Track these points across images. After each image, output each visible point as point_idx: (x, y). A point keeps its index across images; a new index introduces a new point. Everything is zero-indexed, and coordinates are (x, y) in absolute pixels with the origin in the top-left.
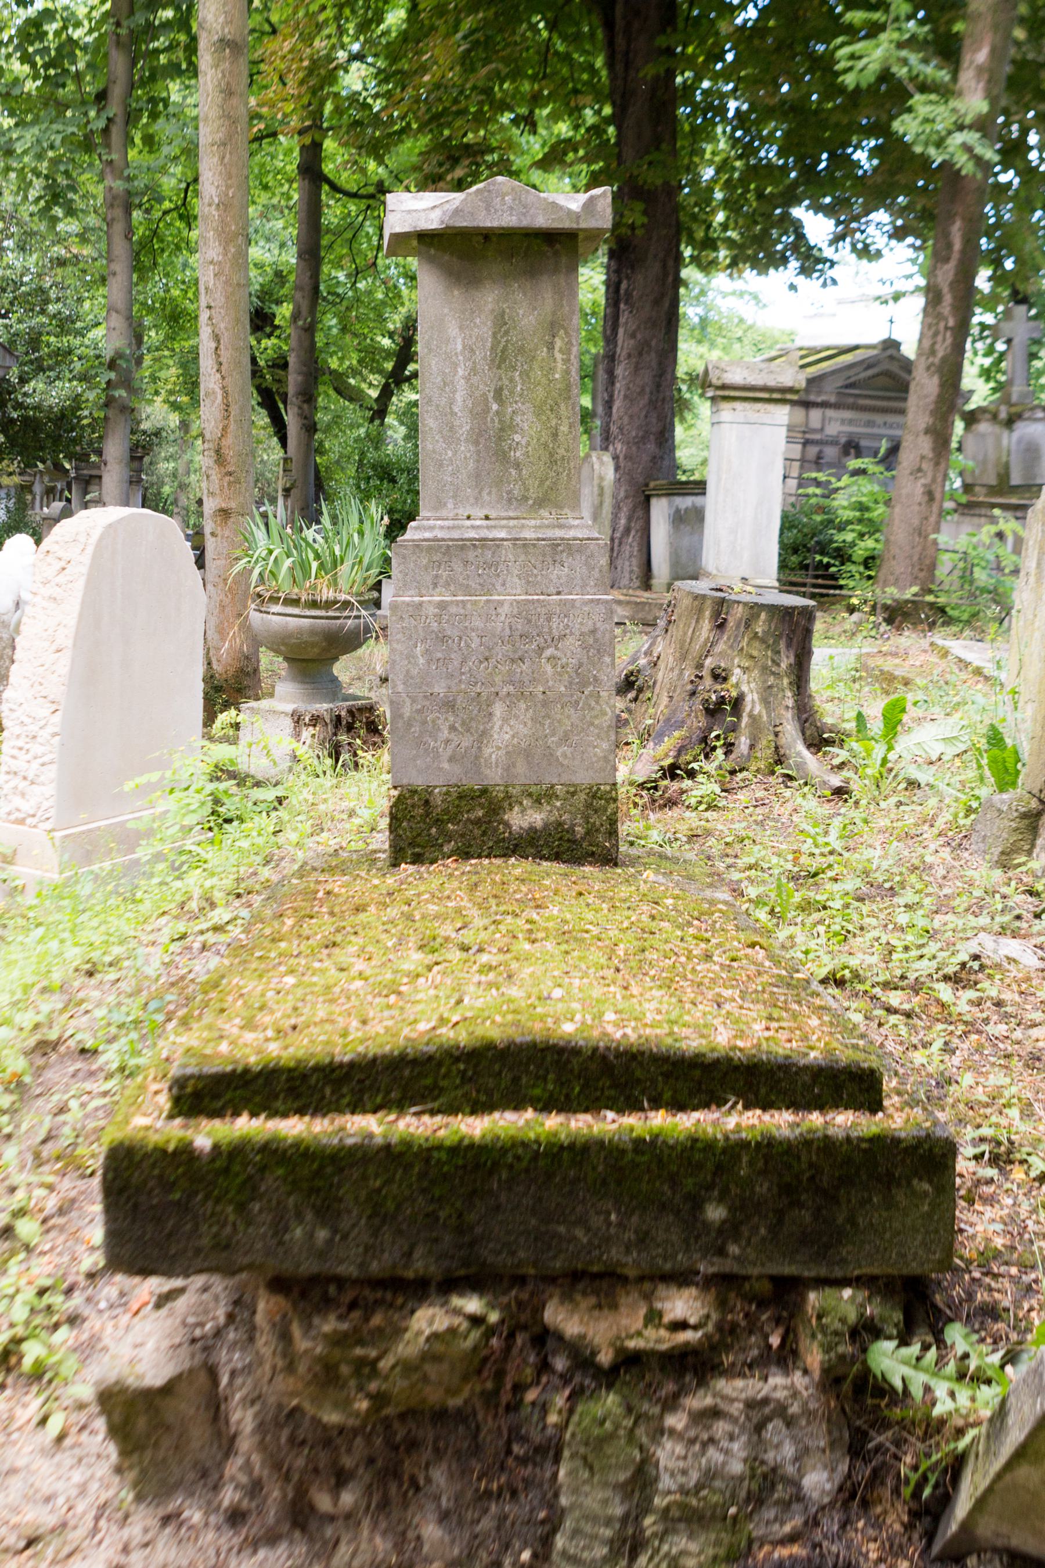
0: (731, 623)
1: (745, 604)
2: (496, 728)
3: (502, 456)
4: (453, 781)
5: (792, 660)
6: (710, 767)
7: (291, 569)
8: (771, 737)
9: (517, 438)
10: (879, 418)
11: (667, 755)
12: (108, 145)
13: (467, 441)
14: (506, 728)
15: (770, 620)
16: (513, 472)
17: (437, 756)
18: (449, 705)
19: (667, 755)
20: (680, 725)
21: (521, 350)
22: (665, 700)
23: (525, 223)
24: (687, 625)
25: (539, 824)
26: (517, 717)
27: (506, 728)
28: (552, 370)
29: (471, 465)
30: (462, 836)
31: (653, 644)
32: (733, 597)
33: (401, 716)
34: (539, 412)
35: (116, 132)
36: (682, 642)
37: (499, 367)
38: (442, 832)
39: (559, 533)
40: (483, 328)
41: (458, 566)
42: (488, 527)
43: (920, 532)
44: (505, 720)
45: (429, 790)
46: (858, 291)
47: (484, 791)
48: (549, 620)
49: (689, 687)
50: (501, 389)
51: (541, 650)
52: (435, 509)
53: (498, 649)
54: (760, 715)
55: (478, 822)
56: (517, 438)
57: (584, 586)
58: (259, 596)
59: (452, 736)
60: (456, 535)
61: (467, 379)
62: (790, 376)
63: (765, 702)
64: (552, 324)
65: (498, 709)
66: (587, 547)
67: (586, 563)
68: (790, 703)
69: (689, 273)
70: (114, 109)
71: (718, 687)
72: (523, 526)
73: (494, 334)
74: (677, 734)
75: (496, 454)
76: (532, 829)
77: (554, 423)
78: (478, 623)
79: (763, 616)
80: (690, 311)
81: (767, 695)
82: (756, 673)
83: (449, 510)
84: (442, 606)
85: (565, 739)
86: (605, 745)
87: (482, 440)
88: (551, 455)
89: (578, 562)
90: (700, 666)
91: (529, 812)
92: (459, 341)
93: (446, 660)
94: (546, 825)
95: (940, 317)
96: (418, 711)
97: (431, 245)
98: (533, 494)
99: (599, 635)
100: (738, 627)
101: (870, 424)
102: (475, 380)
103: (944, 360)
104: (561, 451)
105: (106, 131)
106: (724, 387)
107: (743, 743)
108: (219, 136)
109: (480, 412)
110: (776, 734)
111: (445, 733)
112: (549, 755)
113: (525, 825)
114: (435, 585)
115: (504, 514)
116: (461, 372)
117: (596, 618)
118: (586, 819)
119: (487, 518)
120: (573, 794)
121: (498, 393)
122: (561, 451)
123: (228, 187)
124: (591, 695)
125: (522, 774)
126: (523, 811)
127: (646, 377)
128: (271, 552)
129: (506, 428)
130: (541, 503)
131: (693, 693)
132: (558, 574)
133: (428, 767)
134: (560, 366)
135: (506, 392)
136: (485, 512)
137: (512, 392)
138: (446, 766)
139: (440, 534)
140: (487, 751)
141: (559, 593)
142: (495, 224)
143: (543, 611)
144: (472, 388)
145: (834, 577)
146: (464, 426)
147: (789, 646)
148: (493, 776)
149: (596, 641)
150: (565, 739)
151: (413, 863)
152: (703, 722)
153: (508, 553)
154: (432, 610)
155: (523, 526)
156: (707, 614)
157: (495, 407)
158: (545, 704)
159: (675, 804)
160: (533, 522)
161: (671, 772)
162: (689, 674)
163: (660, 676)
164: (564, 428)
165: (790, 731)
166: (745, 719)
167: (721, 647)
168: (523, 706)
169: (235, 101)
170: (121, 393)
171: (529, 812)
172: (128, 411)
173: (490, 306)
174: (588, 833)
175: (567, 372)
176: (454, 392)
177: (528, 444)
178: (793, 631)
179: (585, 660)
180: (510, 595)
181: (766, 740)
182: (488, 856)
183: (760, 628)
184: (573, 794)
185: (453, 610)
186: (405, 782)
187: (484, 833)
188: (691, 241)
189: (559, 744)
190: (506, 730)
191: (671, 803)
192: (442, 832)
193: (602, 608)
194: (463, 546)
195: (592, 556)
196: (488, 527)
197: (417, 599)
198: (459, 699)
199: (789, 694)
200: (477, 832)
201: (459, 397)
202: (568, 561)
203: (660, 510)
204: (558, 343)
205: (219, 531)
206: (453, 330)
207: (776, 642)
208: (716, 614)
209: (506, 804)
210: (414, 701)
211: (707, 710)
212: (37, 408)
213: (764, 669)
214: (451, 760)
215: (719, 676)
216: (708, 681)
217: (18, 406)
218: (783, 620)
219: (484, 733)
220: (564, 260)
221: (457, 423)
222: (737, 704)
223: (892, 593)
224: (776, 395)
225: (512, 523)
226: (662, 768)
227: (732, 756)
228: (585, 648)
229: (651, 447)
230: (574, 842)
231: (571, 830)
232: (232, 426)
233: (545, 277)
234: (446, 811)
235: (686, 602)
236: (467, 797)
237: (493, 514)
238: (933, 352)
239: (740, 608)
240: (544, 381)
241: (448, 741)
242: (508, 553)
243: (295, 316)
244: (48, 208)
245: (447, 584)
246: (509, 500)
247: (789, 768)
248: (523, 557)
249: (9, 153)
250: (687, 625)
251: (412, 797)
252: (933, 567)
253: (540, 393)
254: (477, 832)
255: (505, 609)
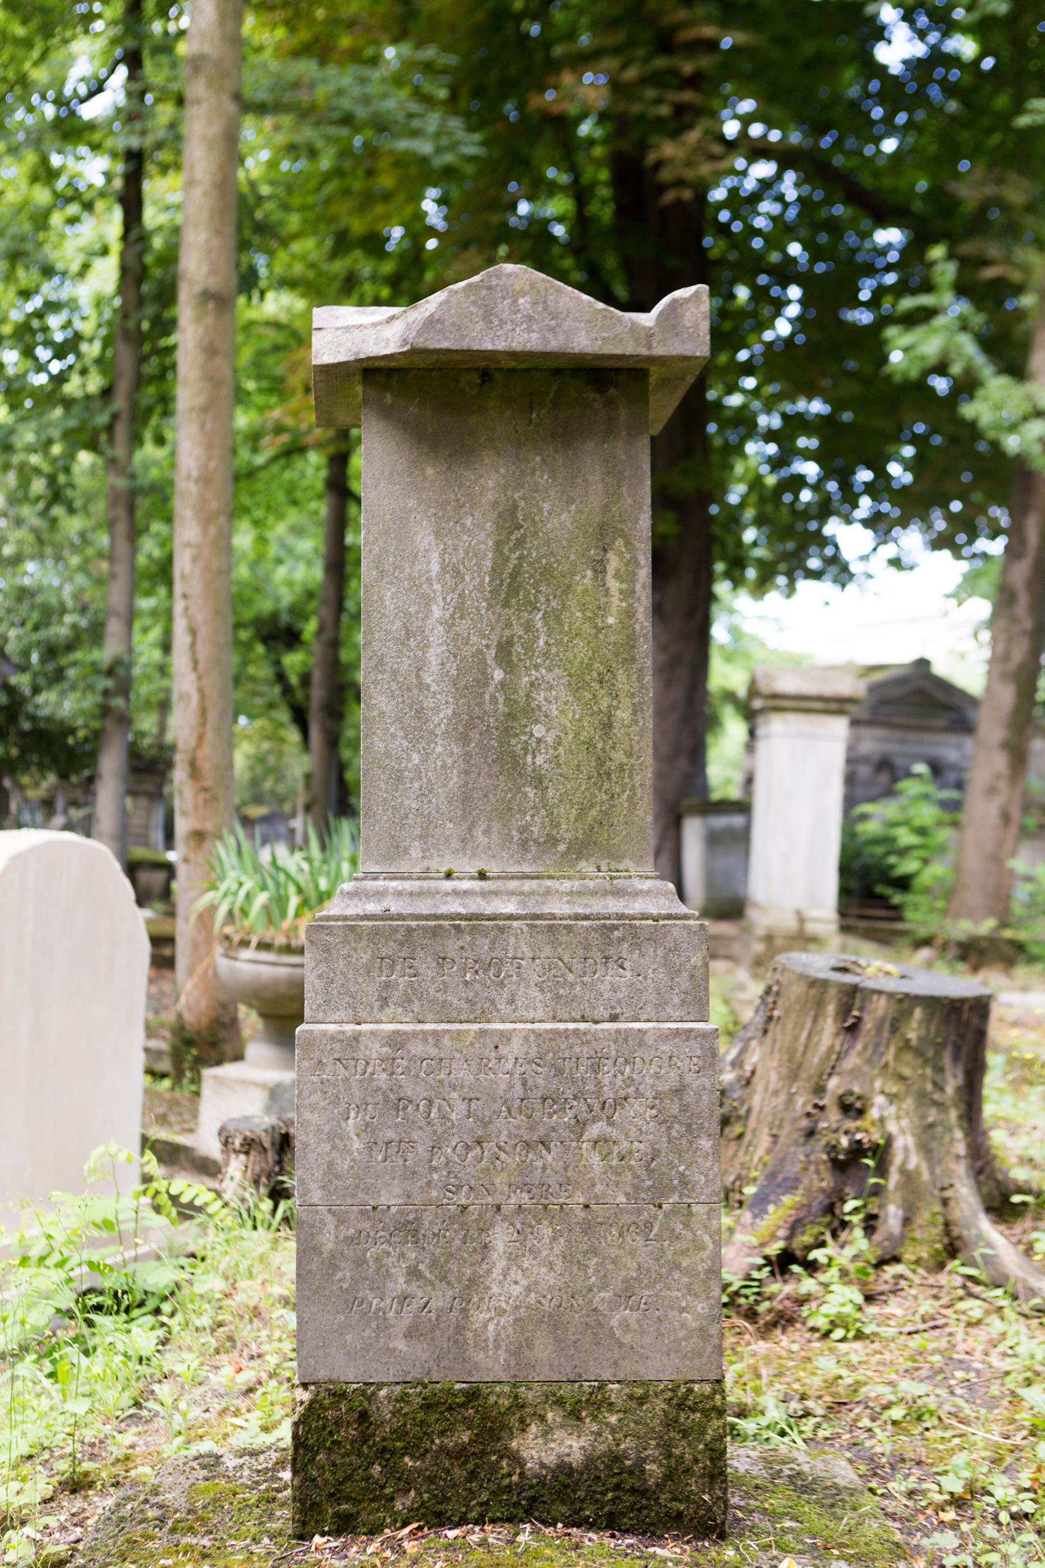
0: (868, 1025)
1: (891, 995)
2: (497, 1273)
3: (510, 764)
4: (414, 1374)
5: (960, 1080)
6: (844, 1257)
7: (266, 908)
8: (937, 1208)
9: (538, 731)
10: (913, 736)
11: (773, 1237)
12: (111, 440)
13: (447, 734)
14: (515, 1274)
15: (927, 1020)
16: (530, 792)
17: (384, 1328)
18: (408, 1229)
19: (773, 1237)
20: (791, 1185)
21: (546, 574)
22: (764, 1141)
23: (554, 344)
24: (799, 1026)
25: (576, 1458)
26: (534, 1252)
27: (515, 1274)
28: (603, 609)
29: (455, 779)
30: (431, 1480)
31: (743, 1051)
32: (870, 984)
33: (317, 1250)
34: (577, 685)
35: (121, 431)
36: (791, 1052)
37: (506, 604)
38: (392, 1471)
39: (614, 906)
40: (479, 535)
41: (427, 968)
42: (484, 894)
43: (996, 859)
44: (513, 1259)
45: (368, 1391)
46: (904, 601)
47: (473, 1395)
48: (596, 1068)
49: (804, 1123)
50: (510, 643)
51: (580, 1125)
52: (388, 858)
53: (500, 1123)
54: (917, 1172)
55: (460, 1454)
56: (538, 731)
57: (660, 1006)
58: (227, 938)
59: (413, 1288)
60: (424, 908)
61: (449, 625)
62: (848, 686)
63: (925, 1148)
64: (602, 527)
65: (500, 1237)
66: (666, 931)
67: (666, 963)
68: (961, 1148)
69: (722, 588)
70: (119, 403)
71: (851, 1124)
72: (548, 892)
73: (498, 546)
74: (787, 1200)
75: (499, 759)
76: (563, 1468)
77: (604, 704)
78: (463, 1074)
79: (918, 1013)
80: (719, 632)
81: (928, 1138)
82: (909, 1103)
83: (414, 860)
84: (397, 1041)
85: (626, 1294)
86: (701, 1307)
87: (474, 735)
88: (600, 762)
89: (650, 959)
90: (820, 1090)
91: (558, 1434)
92: (435, 557)
93: (403, 1144)
94: (590, 1461)
95: (1014, 620)
96: (350, 1240)
97: (386, 387)
98: (566, 833)
99: (689, 1097)
100: (879, 1029)
101: (903, 742)
102: (463, 626)
103: (1021, 667)
104: (619, 756)
105: (110, 428)
106: (775, 696)
107: (892, 1215)
108: (200, 400)
109: (470, 684)
110: (945, 1202)
111: (399, 1283)
112: (595, 1325)
113: (551, 1460)
114: (384, 1002)
115: (514, 869)
116: (437, 612)
117: (684, 1065)
118: (667, 1448)
119: (482, 876)
120: (642, 1400)
121: (505, 649)
122: (619, 756)
123: (209, 459)
124: (675, 1212)
125: (545, 1360)
126: (546, 1434)
127: (678, 692)
128: (241, 884)
129: (519, 713)
130: (580, 850)
131: (811, 1133)
132: (612, 981)
133: (367, 1348)
134: (616, 602)
135: (518, 648)
136: (479, 865)
137: (529, 649)
138: (400, 1344)
139: (395, 906)
140: (479, 1317)
141: (614, 1018)
142: (501, 346)
143: (586, 1051)
144: (456, 642)
145: (896, 908)
146: (442, 709)
147: (956, 1058)
148: (490, 1365)
149: (684, 1108)
150: (626, 1294)
151: (337, 1533)
152: (827, 1182)
153: (520, 943)
154: (376, 1050)
155: (548, 892)
156: (831, 1008)
157: (498, 675)
158: (587, 1228)
159: (791, 1321)
160: (566, 885)
161: (783, 1264)
162: (802, 1102)
163: (756, 1101)
164: (623, 715)
165: (966, 1198)
166: (894, 1178)
167: (852, 1061)
168: (546, 1231)
169: (219, 361)
170: (118, 702)
171: (558, 1434)
172: (125, 721)
173: (491, 496)
174: (669, 1476)
175: (629, 613)
176: (425, 647)
177: (558, 741)
178: (961, 1036)
179: (664, 1145)
180: (523, 1022)
181: (928, 1212)
182: (479, 1521)
183: (913, 1032)
184: (642, 1400)
185: (417, 1048)
186: (322, 1375)
187: (473, 1475)
188: (724, 558)
189: (614, 1306)
190: (515, 1279)
191: (784, 1320)
192: (392, 1471)
193: (694, 1047)
194: (438, 929)
195: (676, 948)
196: (484, 894)
197: (349, 1027)
198: (427, 1218)
199: (959, 1134)
200: (459, 1473)
201: (434, 656)
202: (632, 958)
203: (693, 831)
204: (613, 563)
205: (192, 856)
206: (424, 538)
207: (938, 1054)
208: (845, 1010)
209: (513, 1421)
210: (341, 1220)
211: (834, 1161)
212: (49, 719)
213: (922, 1097)
214: (410, 1334)
215: (851, 1108)
216: (834, 1115)
217: (33, 718)
218: (946, 1019)
219: (473, 1283)
220: (623, 414)
221: (429, 703)
222: (882, 1152)
223: (964, 928)
224: (833, 705)
225: (528, 885)
226: (766, 1257)
227: (877, 1237)
228: (664, 1121)
229: (683, 764)
230: (643, 1493)
231: (638, 1470)
232: (210, 735)
233: (589, 446)
234: (400, 1433)
235: (797, 990)
236: (439, 1405)
237: (493, 868)
238: (1006, 658)
239: (883, 1002)
240: (587, 628)
241: (404, 1298)
242: (520, 943)
243: (321, 630)
244: (48, 507)
245: (406, 1001)
246: (524, 844)
247: (973, 1264)
248: (547, 951)
249: (9, 448)
250: (799, 1026)
251: (335, 1405)
252: (1008, 898)
253: (581, 650)
254: (459, 1473)
255: (516, 1048)
